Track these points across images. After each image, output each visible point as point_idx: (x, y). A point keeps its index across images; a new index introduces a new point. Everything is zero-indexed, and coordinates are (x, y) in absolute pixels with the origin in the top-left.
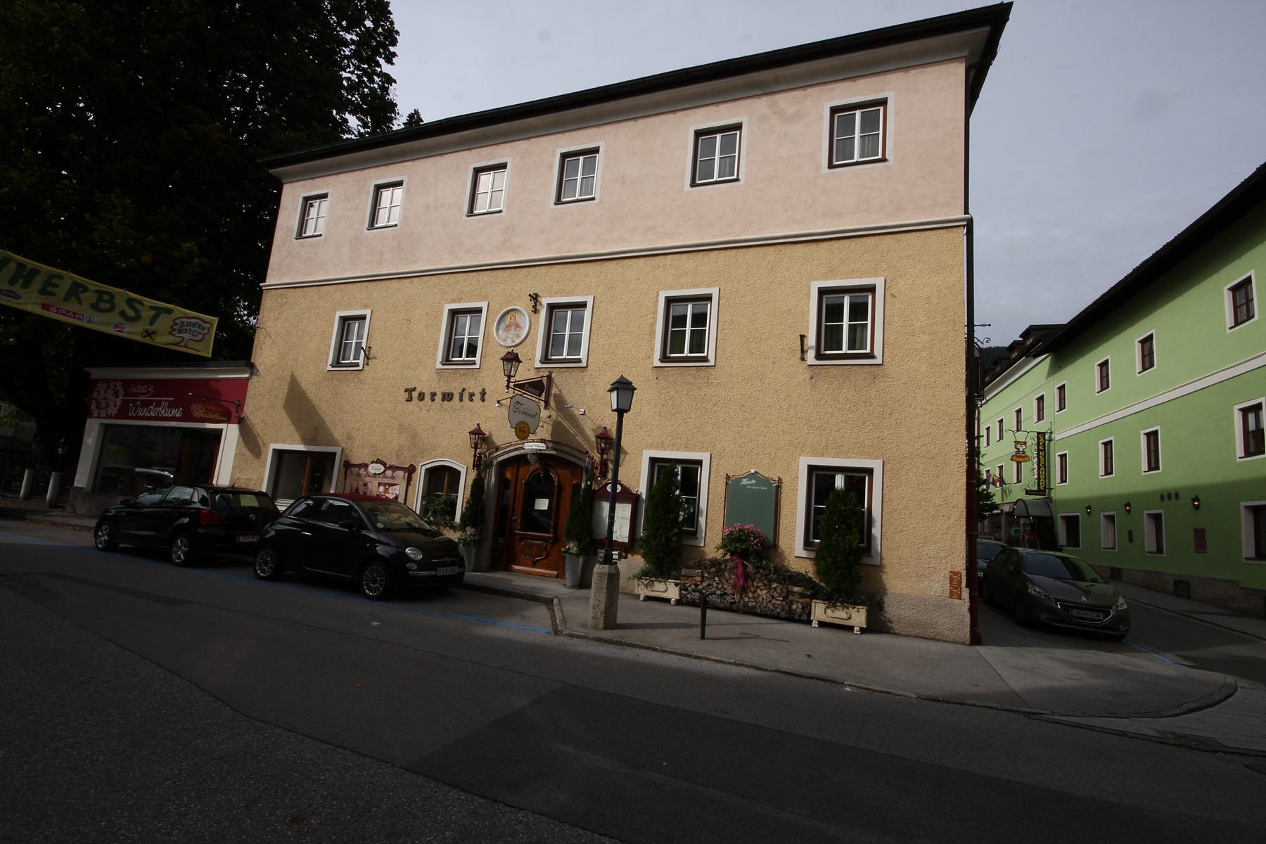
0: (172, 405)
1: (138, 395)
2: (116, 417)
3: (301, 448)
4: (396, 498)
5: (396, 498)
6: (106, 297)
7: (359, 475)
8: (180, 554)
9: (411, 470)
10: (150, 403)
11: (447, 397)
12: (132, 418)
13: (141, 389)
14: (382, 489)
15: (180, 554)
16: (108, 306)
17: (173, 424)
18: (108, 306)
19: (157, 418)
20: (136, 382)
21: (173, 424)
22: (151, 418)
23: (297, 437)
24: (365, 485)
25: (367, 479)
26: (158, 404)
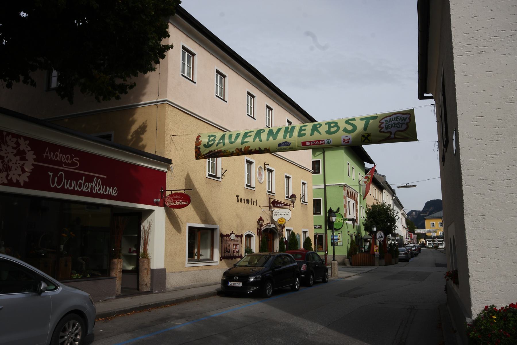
0: (106, 183)
1: (60, 163)
2: (27, 185)
3: (202, 226)
4: (201, 255)
5: (201, 255)
6: (332, 125)
7: (227, 241)
8: (269, 292)
9: (241, 236)
10: (80, 176)
11: (248, 201)
12: (55, 190)
13: (60, 157)
14: (234, 247)
15: (269, 292)
16: (335, 129)
17: (107, 202)
18: (335, 129)
19: (90, 194)
20: (54, 148)
21: (107, 202)
22: (82, 194)
23: (199, 220)
24: (229, 246)
25: (229, 243)
26: (89, 179)
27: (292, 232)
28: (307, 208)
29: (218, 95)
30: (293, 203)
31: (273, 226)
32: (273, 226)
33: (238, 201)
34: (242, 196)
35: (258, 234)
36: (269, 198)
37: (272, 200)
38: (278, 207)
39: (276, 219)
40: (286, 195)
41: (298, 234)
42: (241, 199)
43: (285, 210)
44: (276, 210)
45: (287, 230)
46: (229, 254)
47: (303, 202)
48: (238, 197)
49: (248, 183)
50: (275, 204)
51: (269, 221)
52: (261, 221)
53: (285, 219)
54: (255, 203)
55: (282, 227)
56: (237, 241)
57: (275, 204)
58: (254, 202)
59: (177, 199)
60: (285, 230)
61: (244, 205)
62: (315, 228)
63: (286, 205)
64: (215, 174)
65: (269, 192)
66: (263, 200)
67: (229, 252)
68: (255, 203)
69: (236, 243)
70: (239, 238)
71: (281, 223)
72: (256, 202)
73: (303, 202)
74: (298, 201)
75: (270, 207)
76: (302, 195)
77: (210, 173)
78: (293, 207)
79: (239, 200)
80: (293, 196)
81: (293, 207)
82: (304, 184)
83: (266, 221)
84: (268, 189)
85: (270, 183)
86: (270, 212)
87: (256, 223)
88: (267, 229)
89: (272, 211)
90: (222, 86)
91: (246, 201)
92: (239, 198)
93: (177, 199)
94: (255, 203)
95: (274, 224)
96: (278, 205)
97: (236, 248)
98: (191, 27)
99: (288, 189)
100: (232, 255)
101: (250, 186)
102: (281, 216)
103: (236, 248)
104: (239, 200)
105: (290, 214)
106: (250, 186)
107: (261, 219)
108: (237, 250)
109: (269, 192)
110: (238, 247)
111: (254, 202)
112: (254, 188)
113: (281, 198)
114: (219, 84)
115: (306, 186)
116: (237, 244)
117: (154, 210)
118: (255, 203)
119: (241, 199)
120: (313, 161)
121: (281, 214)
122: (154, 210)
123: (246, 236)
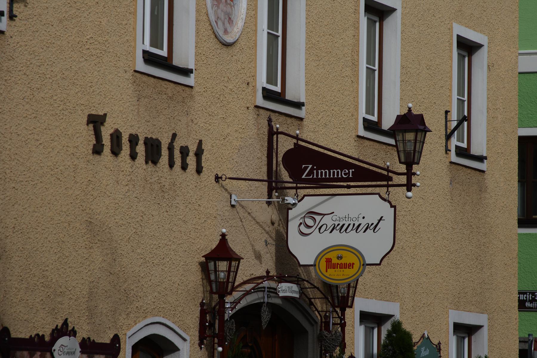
27: (397, 326)
28: (482, 189)
30: (411, 160)
31: (288, 290)
32: (288, 290)
33: (97, 150)
34: (123, 119)
35: (206, 334)
36: (272, 133)
37: (285, 145)
38: (318, 183)
39: (305, 249)
40: (362, 113)
41: (426, 340)
42: (116, 137)
43: (364, 205)
44: (308, 203)
45: (365, 317)
47: (462, 153)
48: (96, 121)
49: (156, 41)
50: (305, 166)
51: (268, 264)
52: (223, 265)
54: (191, 160)
55: (340, 299)
57: (305, 166)
58: (185, 151)
60: (352, 316)
61: (123, 171)
62: (522, 305)
63: (364, 176)
64: (164, 53)
65: (268, 95)
66: (235, 144)
68: (191, 160)
71: (335, 276)
72: (199, 154)
73: (462, 153)
74: (434, 156)
75: (274, 185)
76: (454, 116)
77: (148, 48)
78: (409, 186)
79: (106, 141)
80: (411, 124)
81: (409, 186)
82: (467, 48)
83: (254, 264)
84: (262, 81)
85: (278, 44)
86: (268, 214)
87: (195, 277)
88: (256, 308)
89: (284, 210)
91: (141, 149)
92: (106, 132)
94: (191, 158)
95: (296, 280)
96: (323, 173)
99: (376, 76)
101: (164, 63)
104: (106, 141)
105: (387, 226)
106: (164, 63)
107: (222, 251)
109: (268, 95)
111: (185, 151)
112: (186, 72)
113: (336, 132)
115: (481, 59)
118: (191, 158)
119: (116, 137)
120: (522, 140)
121: (332, 226)
123: (135, 348)
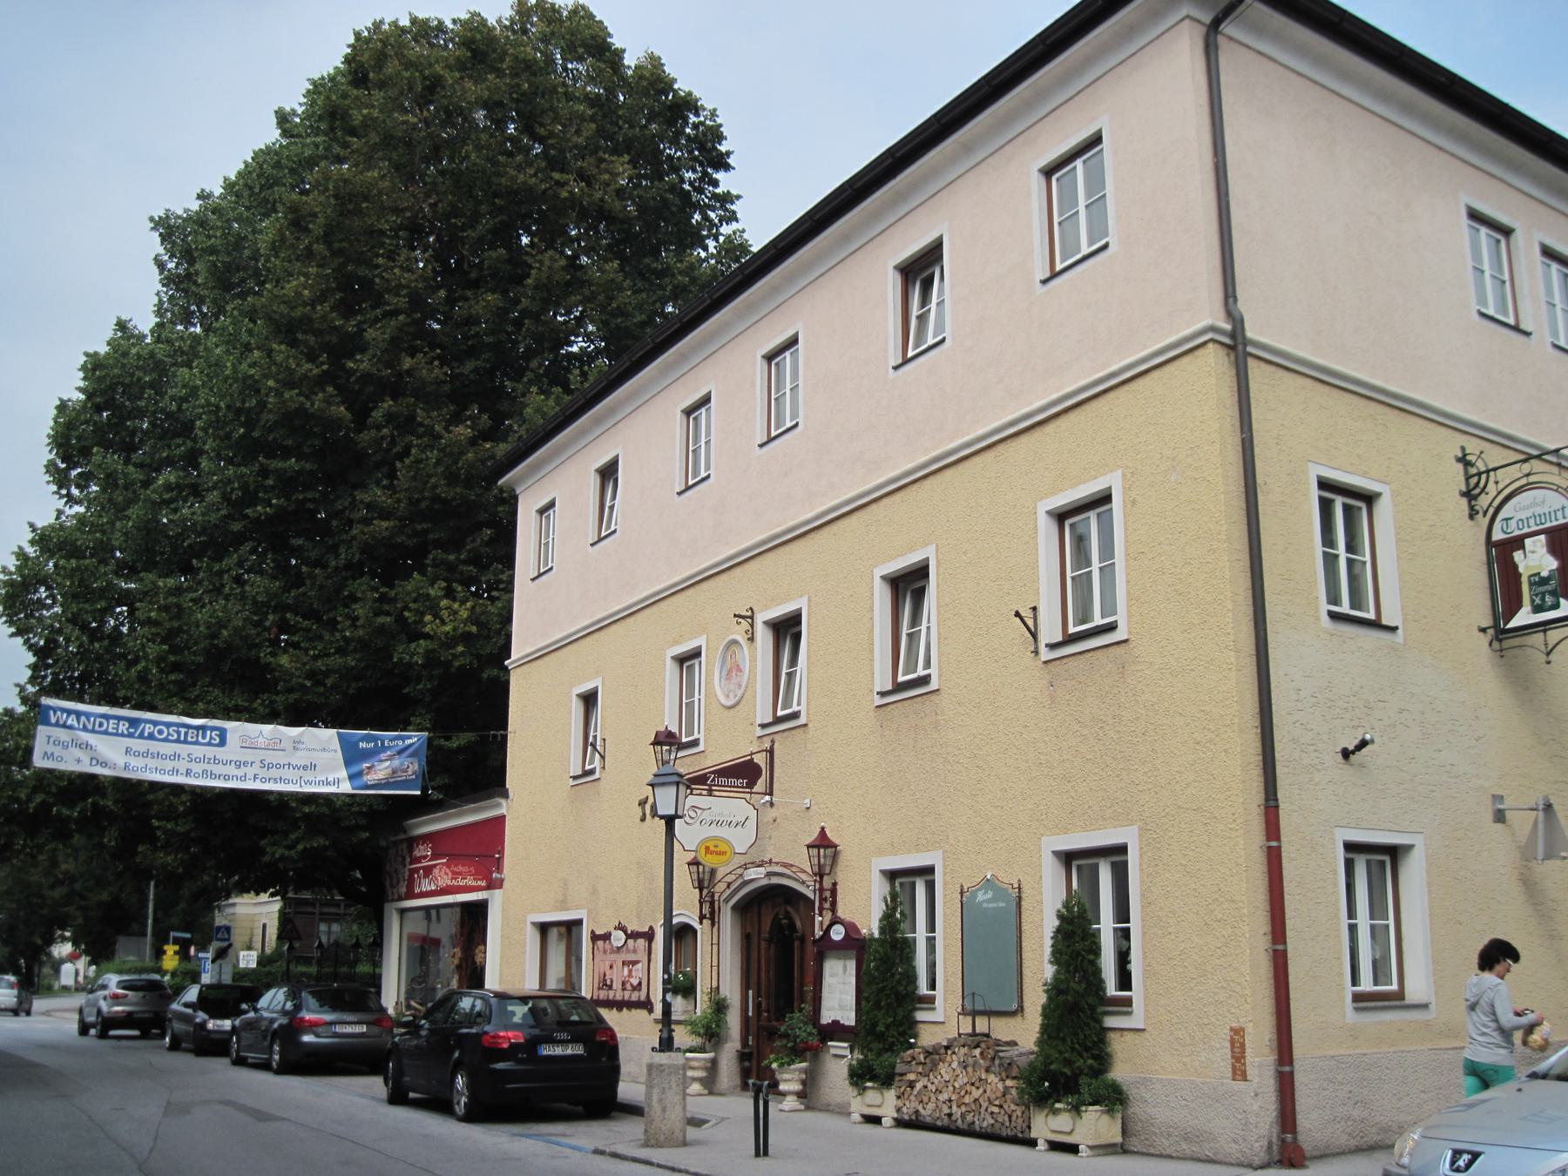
29: (1491, 312)
33: (643, 819)
37: (760, 785)
46: (611, 994)
53: (728, 842)
56: (635, 951)
59: (459, 873)
67: (610, 987)
69: (631, 957)
70: (641, 942)
90: (1500, 270)
93: (459, 873)
97: (630, 975)
98: (1110, 222)
100: (619, 998)
102: (715, 831)
103: (630, 975)
108: (635, 982)
110: (639, 971)
114: (1486, 267)
116: (634, 963)
117: (1411, 847)
122: (1411, 847)
